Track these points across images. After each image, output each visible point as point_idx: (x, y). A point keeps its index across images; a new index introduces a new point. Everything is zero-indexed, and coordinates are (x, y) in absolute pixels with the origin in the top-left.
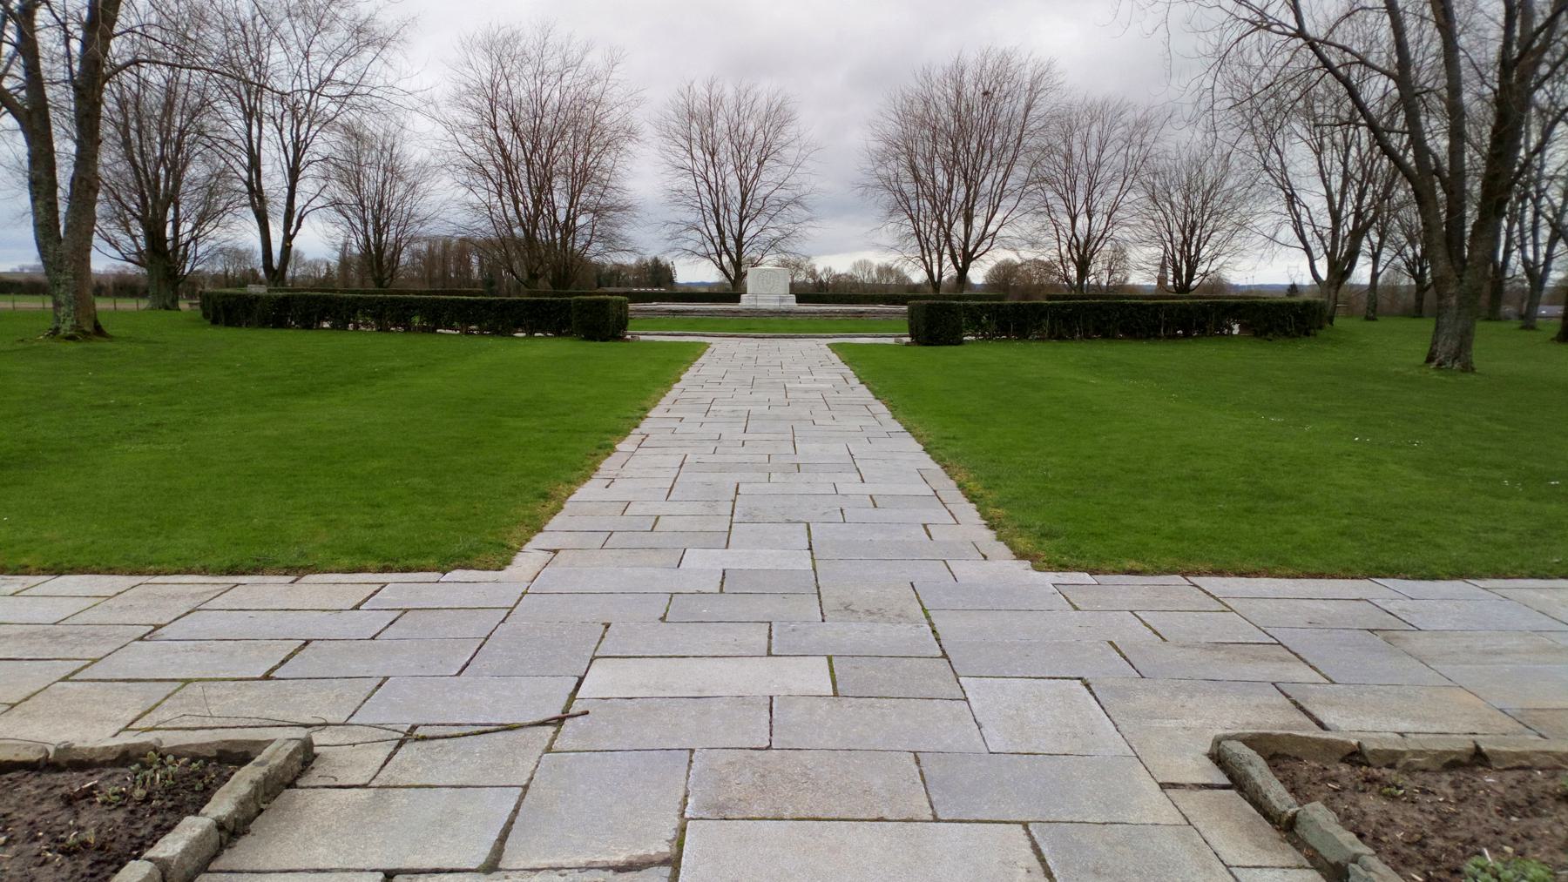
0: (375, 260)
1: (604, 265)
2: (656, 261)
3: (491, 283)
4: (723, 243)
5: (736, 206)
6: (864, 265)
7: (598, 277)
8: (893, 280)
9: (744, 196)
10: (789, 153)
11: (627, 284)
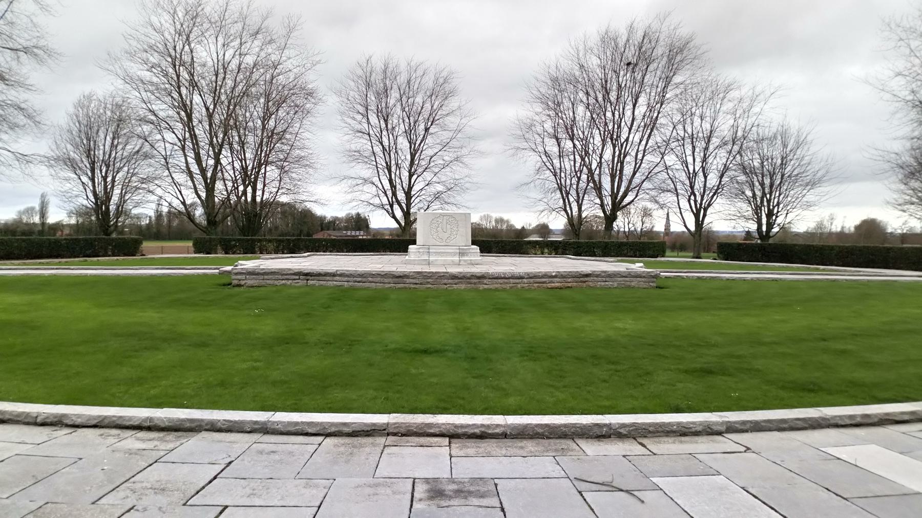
0: (765, 237)
1: (325, 218)
2: (358, 214)
4: (394, 194)
6: (487, 217)
8: (504, 227)
9: (413, 156)
10: (452, 122)
11: (340, 229)
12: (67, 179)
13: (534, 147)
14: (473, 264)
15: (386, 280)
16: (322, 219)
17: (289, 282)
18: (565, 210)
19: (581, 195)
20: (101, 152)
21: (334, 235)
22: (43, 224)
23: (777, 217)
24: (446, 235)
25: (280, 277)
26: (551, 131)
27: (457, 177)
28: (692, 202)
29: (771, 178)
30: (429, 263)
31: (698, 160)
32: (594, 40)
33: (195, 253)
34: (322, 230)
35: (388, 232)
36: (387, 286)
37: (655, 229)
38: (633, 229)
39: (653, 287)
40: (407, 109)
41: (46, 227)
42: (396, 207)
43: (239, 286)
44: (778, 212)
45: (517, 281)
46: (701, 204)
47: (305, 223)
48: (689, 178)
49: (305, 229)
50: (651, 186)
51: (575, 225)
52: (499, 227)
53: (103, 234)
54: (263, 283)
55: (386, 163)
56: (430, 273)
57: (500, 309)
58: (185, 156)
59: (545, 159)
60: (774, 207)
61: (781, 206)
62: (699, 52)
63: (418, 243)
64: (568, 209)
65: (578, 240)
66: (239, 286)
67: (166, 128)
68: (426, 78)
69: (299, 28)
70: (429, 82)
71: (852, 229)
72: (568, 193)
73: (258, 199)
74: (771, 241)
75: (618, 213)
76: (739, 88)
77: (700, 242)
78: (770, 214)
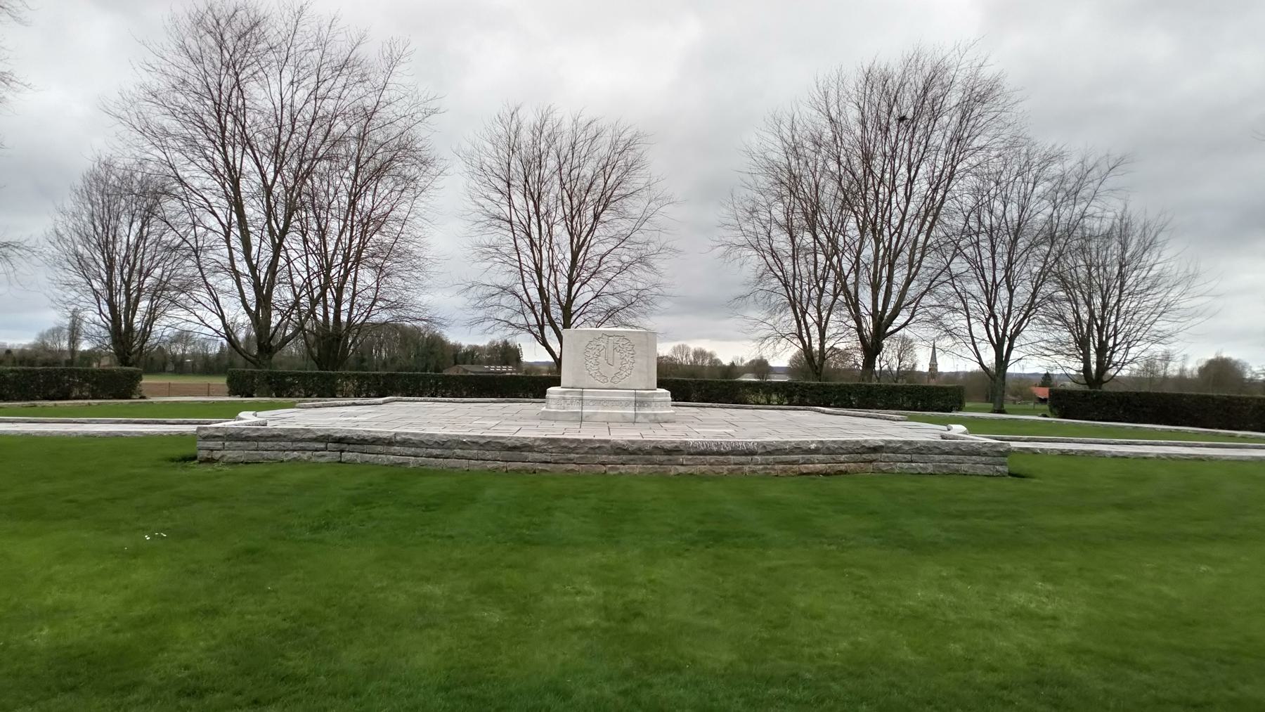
0: (1094, 378)
3: (363, 360)
4: (546, 310)
6: (682, 349)
7: (455, 356)
9: (575, 256)
10: (635, 207)
11: (480, 363)
12: (72, 285)
13: (754, 242)
14: (658, 421)
15: (489, 455)
16: (456, 348)
17: (305, 456)
18: (801, 337)
19: (824, 314)
20: (124, 246)
21: (472, 370)
22: (73, 351)
23: (1113, 352)
24: (613, 370)
26: (781, 218)
27: (640, 286)
28: (991, 328)
29: (1103, 298)
30: (581, 419)
32: (853, 81)
33: (232, 393)
34: (456, 363)
35: (546, 368)
36: (490, 465)
37: (918, 368)
38: (886, 367)
39: (1002, 475)
40: (567, 186)
41: (77, 356)
42: (548, 330)
43: (210, 461)
44: (1115, 345)
45: (743, 459)
46: (1005, 330)
47: (432, 353)
48: (986, 293)
50: (935, 302)
51: (811, 362)
52: (700, 363)
53: (123, 367)
54: (256, 455)
55: (535, 264)
57: (715, 535)
58: (230, 248)
60: (1108, 338)
61: (1120, 337)
65: (812, 385)
66: (210, 461)
67: (202, 206)
68: (600, 141)
71: (1196, 373)
72: (804, 313)
73: (344, 318)
74: (1106, 388)
75: (885, 342)
77: (994, 387)
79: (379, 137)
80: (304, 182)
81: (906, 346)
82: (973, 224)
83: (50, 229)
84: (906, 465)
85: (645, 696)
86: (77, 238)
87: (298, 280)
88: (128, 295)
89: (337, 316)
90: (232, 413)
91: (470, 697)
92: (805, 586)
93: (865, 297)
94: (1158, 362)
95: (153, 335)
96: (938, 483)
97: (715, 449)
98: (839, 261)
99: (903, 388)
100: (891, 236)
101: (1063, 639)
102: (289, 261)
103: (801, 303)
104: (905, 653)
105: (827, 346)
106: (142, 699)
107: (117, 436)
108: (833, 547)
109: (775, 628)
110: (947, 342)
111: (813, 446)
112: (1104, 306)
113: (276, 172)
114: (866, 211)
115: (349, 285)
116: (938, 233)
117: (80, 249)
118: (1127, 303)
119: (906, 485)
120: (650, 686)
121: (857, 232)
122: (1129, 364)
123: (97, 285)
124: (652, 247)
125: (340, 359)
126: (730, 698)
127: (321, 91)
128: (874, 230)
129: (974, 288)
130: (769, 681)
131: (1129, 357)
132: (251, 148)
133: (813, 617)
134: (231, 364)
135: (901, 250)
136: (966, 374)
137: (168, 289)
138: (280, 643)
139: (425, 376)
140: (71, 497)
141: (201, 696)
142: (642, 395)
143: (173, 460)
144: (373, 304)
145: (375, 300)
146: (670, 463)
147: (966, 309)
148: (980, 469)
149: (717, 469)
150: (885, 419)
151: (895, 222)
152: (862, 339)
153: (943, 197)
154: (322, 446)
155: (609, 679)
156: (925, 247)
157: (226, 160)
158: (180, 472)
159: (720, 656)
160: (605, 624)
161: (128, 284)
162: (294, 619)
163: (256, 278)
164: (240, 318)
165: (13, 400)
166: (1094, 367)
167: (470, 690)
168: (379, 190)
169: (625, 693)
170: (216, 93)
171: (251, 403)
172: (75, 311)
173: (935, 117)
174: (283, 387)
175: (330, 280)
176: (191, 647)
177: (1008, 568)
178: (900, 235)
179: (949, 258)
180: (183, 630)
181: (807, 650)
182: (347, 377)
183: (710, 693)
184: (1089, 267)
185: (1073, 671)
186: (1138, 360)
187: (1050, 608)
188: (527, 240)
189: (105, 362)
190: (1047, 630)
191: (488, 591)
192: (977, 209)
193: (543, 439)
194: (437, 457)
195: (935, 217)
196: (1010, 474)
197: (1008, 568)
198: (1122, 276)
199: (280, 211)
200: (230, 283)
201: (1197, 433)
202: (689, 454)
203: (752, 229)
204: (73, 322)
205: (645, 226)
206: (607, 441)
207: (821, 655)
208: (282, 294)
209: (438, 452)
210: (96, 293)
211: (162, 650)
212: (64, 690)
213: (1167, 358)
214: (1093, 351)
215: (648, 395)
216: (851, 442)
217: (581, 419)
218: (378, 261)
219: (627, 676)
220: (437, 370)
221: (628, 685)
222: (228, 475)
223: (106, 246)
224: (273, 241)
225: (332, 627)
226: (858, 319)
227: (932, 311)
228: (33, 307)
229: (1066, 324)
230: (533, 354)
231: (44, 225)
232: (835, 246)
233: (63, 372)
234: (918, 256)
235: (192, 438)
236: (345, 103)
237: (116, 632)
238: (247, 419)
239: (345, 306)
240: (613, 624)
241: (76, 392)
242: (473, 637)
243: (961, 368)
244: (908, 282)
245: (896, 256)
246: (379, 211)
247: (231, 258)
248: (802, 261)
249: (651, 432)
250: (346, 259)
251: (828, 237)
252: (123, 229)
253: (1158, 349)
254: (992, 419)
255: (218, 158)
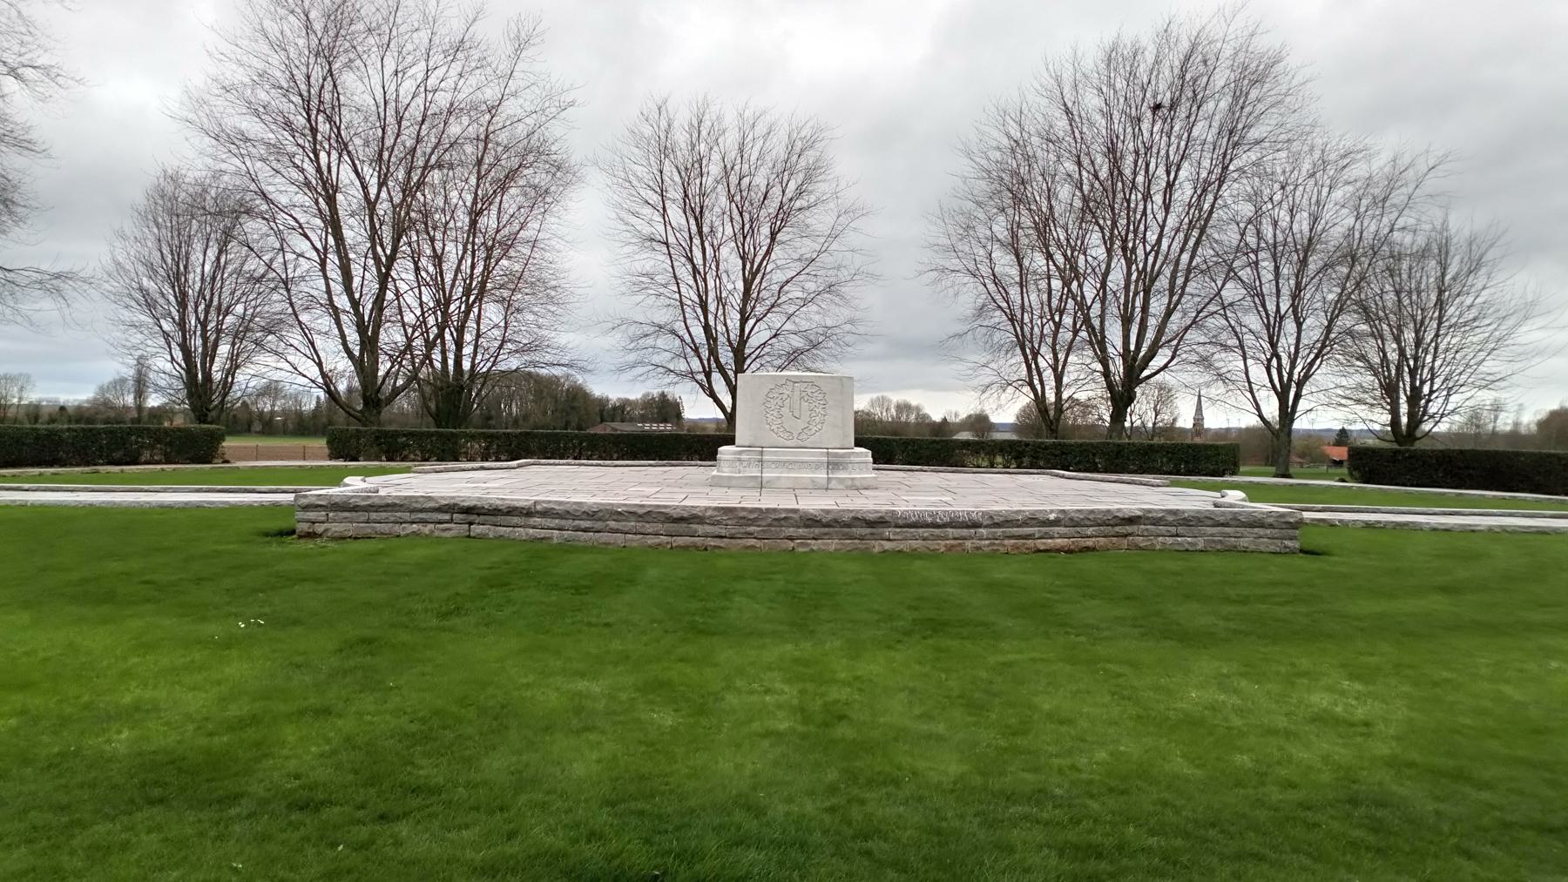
0: (1404, 434)
1: (608, 400)
2: (663, 395)
3: (490, 418)
4: (713, 352)
5: (736, 300)
6: (882, 402)
7: (602, 411)
10: (820, 220)
11: (632, 420)
13: (972, 267)
14: (856, 487)
15: (649, 528)
16: (602, 403)
17: (427, 529)
18: (1031, 384)
19: (1061, 356)
22: (140, 408)
23: (1429, 401)
24: (801, 424)
25: (406, 516)
27: (829, 323)
28: (1274, 372)
29: (1417, 332)
31: (1285, 291)
32: (1092, 59)
34: (602, 421)
35: (713, 426)
36: (651, 540)
37: (1179, 424)
38: (1138, 423)
40: (738, 198)
41: (145, 414)
42: (716, 377)
43: (311, 535)
44: (1432, 392)
45: (965, 532)
46: (1291, 374)
48: (1268, 326)
49: (574, 420)
50: (1202, 339)
52: (903, 419)
53: (201, 427)
54: (368, 529)
55: (700, 296)
56: (753, 510)
57: (934, 623)
58: (326, 278)
59: (991, 287)
60: (1423, 382)
61: (1438, 381)
62: (1295, 82)
63: (737, 441)
64: (1036, 382)
66: (311, 535)
69: (537, 40)
70: (778, 149)
71: (1534, 428)
72: (1036, 354)
73: (466, 365)
74: (1418, 445)
75: (1138, 390)
76: (1368, 159)
77: (1276, 447)
78: (1415, 397)
79: (503, 137)
80: (414, 197)
81: (1165, 396)
82: (1251, 240)
83: (106, 260)
84: (1170, 540)
85: (856, 813)
86: (141, 269)
87: (409, 318)
88: (205, 339)
89: (458, 362)
90: (336, 479)
91: (641, 813)
92: (1049, 684)
93: (1114, 333)
94: (1485, 413)
95: (235, 387)
96: (1212, 562)
97: (930, 520)
98: (1080, 286)
99: (1162, 447)
100: (1147, 255)
101: (1383, 749)
102: (398, 295)
103: (1031, 342)
104: (1178, 765)
105: (1065, 396)
106: (245, 812)
107: (198, 506)
108: (1083, 639)
109: (1014, 734)
110: (1218, 389)
111: (1052, 517)
112: (1418, 342)
113: (380, 185)
114: (1114, 224)
115: (471, 324)
116: (1205, 251)
117: (145, 282)
118: (1448, 338)
119: (1171, 565)
120: (862, 802)
121: (1102, 250)
122: (1447, 419)
123: (167, 326)
124: (844, 274)
125: (461, 417)
126: (962, 817)
127: (432, 82)
128: (1124, 249)
129: (1253, 321)
130: (1010, 798)
131: (1450, 407)
132: (349, 153)
133: (1061, 723)
134: (330, 423)
135: (1159, 273)
136: (1240, 430)
137: (252, 330)
138: (408, 748)
139: (567, 435)
140: (147, 578)
141: (317, 810)
142: (836, 455)
143: (267, 535)
144: (500, 347)
145: (503, 342)
146: (874, 537)
147: (1242, 347)
148: (1265, 544)
149: (932, 545)
150: (1141, 484)
151: (1152, 237)
152: (1110, 386)
153: (1213, 206)
154: (447, 517)
155: (811, 793)
156: (1189, 270)
157: (319, 170)
158: (275, 548)
159: (949, 767)
160: (801, 728)
161: (204, 325)
162: (423, 720)
163: (359, 316)
164: (341, 366)
165: (71, 465)
166: (1404, 420)
167: (640, 805)
168: (505, 205)
169: (832, 810)
170: (303, 87)
171: (357, 468)
172: (141, 357)
173: (1198, 102)
174: (394, 448)
175: (451, 317)
176: (302, 753)
177: (1304, 663)
178: (1157, 253)
179: (1220, 283)
180: (290, 733)
181: (1056, 761)
182: (473, 437)
183: (937, 811)
184: (1398, 293)
185: (1394, 788)
186: (1462, 410)
187: (1360, 713)
188: (689, 267)
189: (179, 421)
190: (1359, 739)
191: (657, 688)
192: (1255, 220)
193: (716, 509)
194: (585, 530)
195: (1202, 231)
196: (1302, 551)
197: (1304, 663)
198: (1441, 304)
199: (387, 234)
200: (326, 322)
201: (1537, 501)
202: (897, 526)
203: (967, 249)
204: (139, 372)
205: (834, 246)
206: (795, 511)
207: (1073, 767)
208: (391, 336)
209: (587, 524)
210: (166, 335)
211: (265, 756)
212: (152, 802)
213: (1497, 408)
214: (1403, 399)
215: (843, 456)
216: (1100, 511)
217: (761, 485)
218: (506, 293)
219: (833, 790)
220: (580, 428)
221: (834, 801)
222: (334, 551)
223: (177, 278)
224: (379, 270)
225: (470, 730)
226: (1104, 361)
227: (1201, 349)
228: (88, 357)
229: (1371, 367)
230: (698, 409)
231: (101, 249)
232: (1074, 268)
233: (130, 432)
234: (1180, 281)
235: (289, 509)
236: (461, 96)
237: (211, 734)
238: (354, 485)
239: (467, 350)
240: (812, 728)
241: (146, 455)
242: (640, 742)
243: (1234, 424)
244: (1169, 313)
245: (1153, 281)
246: (505, 232)
247: (329, 291)
248: (1032, 287)
249: (848, 500)
250: (467, 292)
251: (1065, 255)
252: (196, 257)
253: (1486, 397)
254: (1276, 485)
255: (310, 169)
